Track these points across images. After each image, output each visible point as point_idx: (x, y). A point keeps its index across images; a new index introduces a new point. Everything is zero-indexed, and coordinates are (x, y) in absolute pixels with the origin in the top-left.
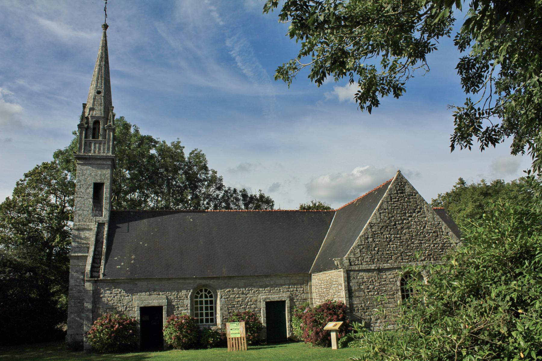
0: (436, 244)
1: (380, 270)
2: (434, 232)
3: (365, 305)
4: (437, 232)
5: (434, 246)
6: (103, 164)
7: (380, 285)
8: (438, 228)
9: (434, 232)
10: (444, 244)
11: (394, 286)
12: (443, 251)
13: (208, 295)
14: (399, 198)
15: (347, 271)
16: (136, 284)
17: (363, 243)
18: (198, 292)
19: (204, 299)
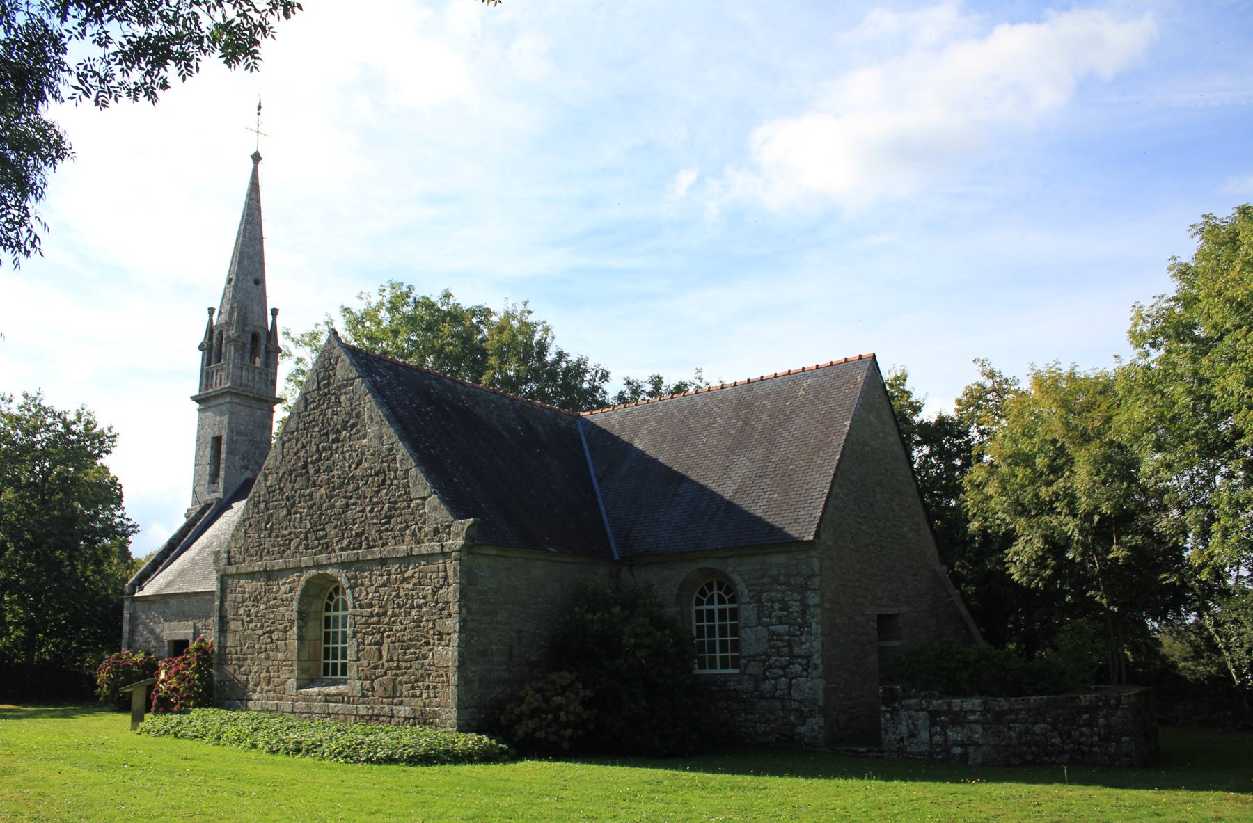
0: (377, 503)
1: (269, 575)
2: (377, 474)
3: (242, 650)
4: (384, 472)
5: (372, 511)
6: (221, 404)
7: (266, 609)
8: (386, 461)
9: (377, 474)
10: (395, 503)
11: (288, 611)
12: (389, 523)
13: (726, 598)
14: (319, 400)
15: (222, 576)
16: (168, 603)
17: (250, 516)
18: (703, 589)
19: (716, 607)
